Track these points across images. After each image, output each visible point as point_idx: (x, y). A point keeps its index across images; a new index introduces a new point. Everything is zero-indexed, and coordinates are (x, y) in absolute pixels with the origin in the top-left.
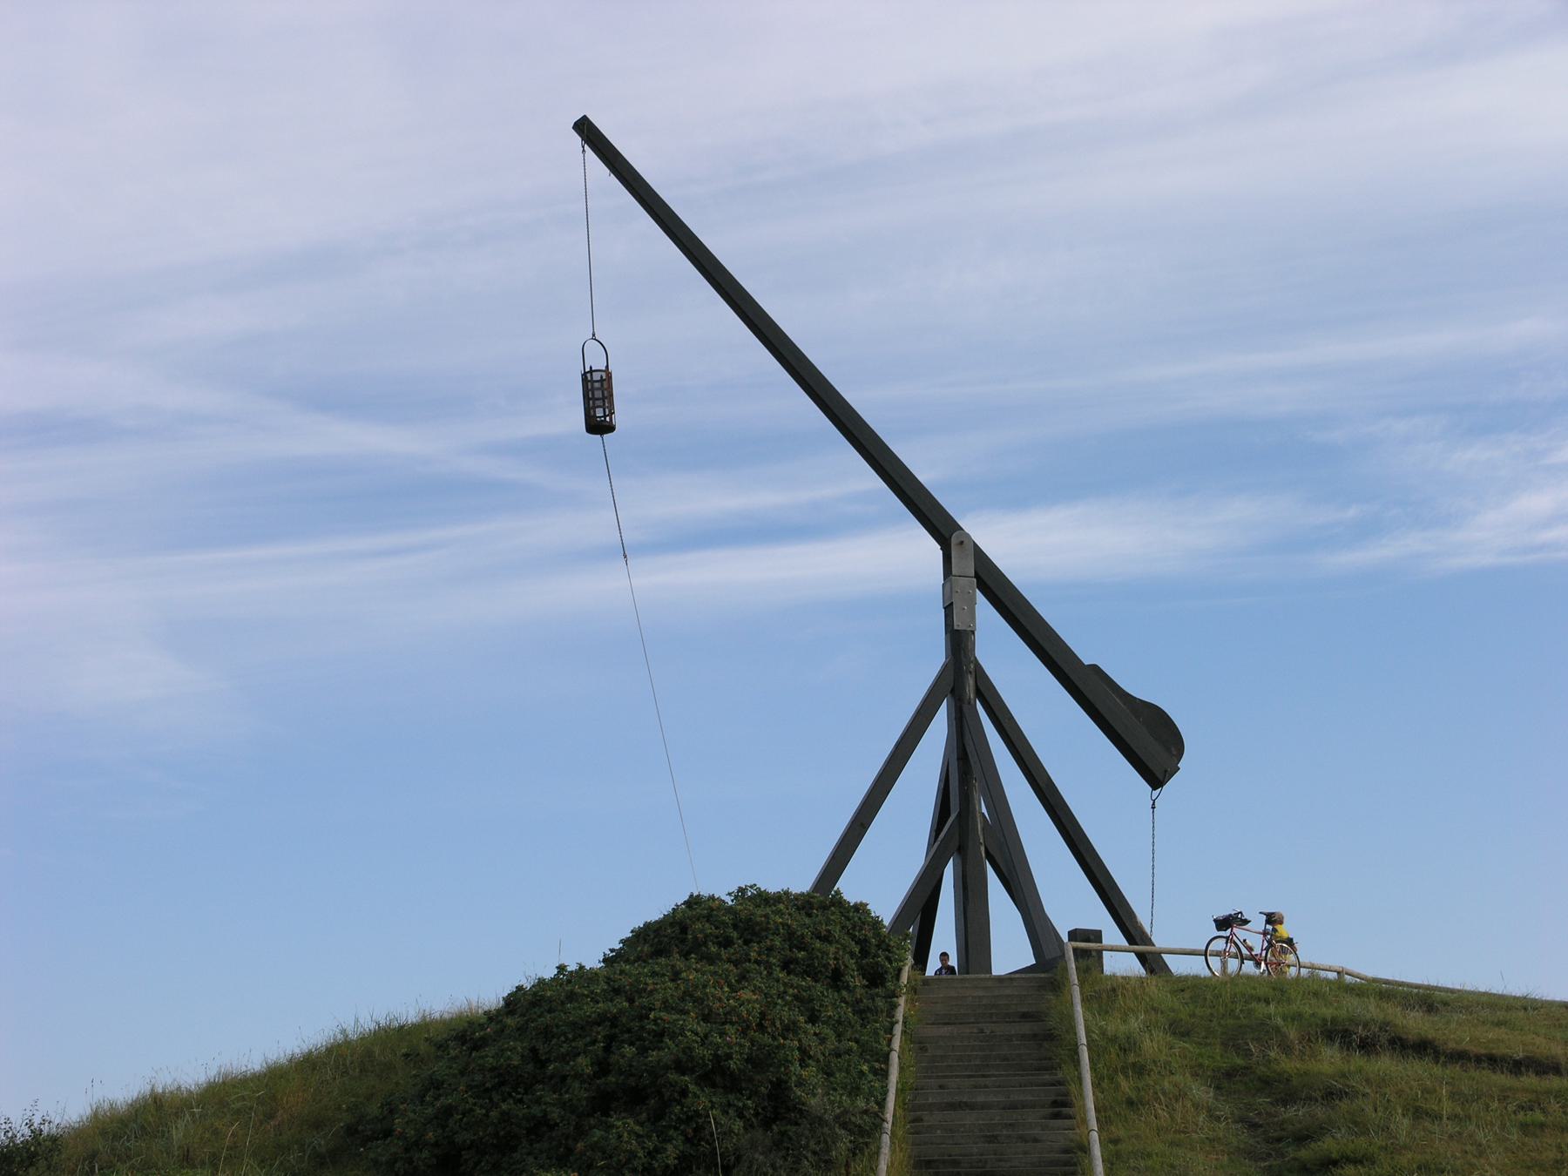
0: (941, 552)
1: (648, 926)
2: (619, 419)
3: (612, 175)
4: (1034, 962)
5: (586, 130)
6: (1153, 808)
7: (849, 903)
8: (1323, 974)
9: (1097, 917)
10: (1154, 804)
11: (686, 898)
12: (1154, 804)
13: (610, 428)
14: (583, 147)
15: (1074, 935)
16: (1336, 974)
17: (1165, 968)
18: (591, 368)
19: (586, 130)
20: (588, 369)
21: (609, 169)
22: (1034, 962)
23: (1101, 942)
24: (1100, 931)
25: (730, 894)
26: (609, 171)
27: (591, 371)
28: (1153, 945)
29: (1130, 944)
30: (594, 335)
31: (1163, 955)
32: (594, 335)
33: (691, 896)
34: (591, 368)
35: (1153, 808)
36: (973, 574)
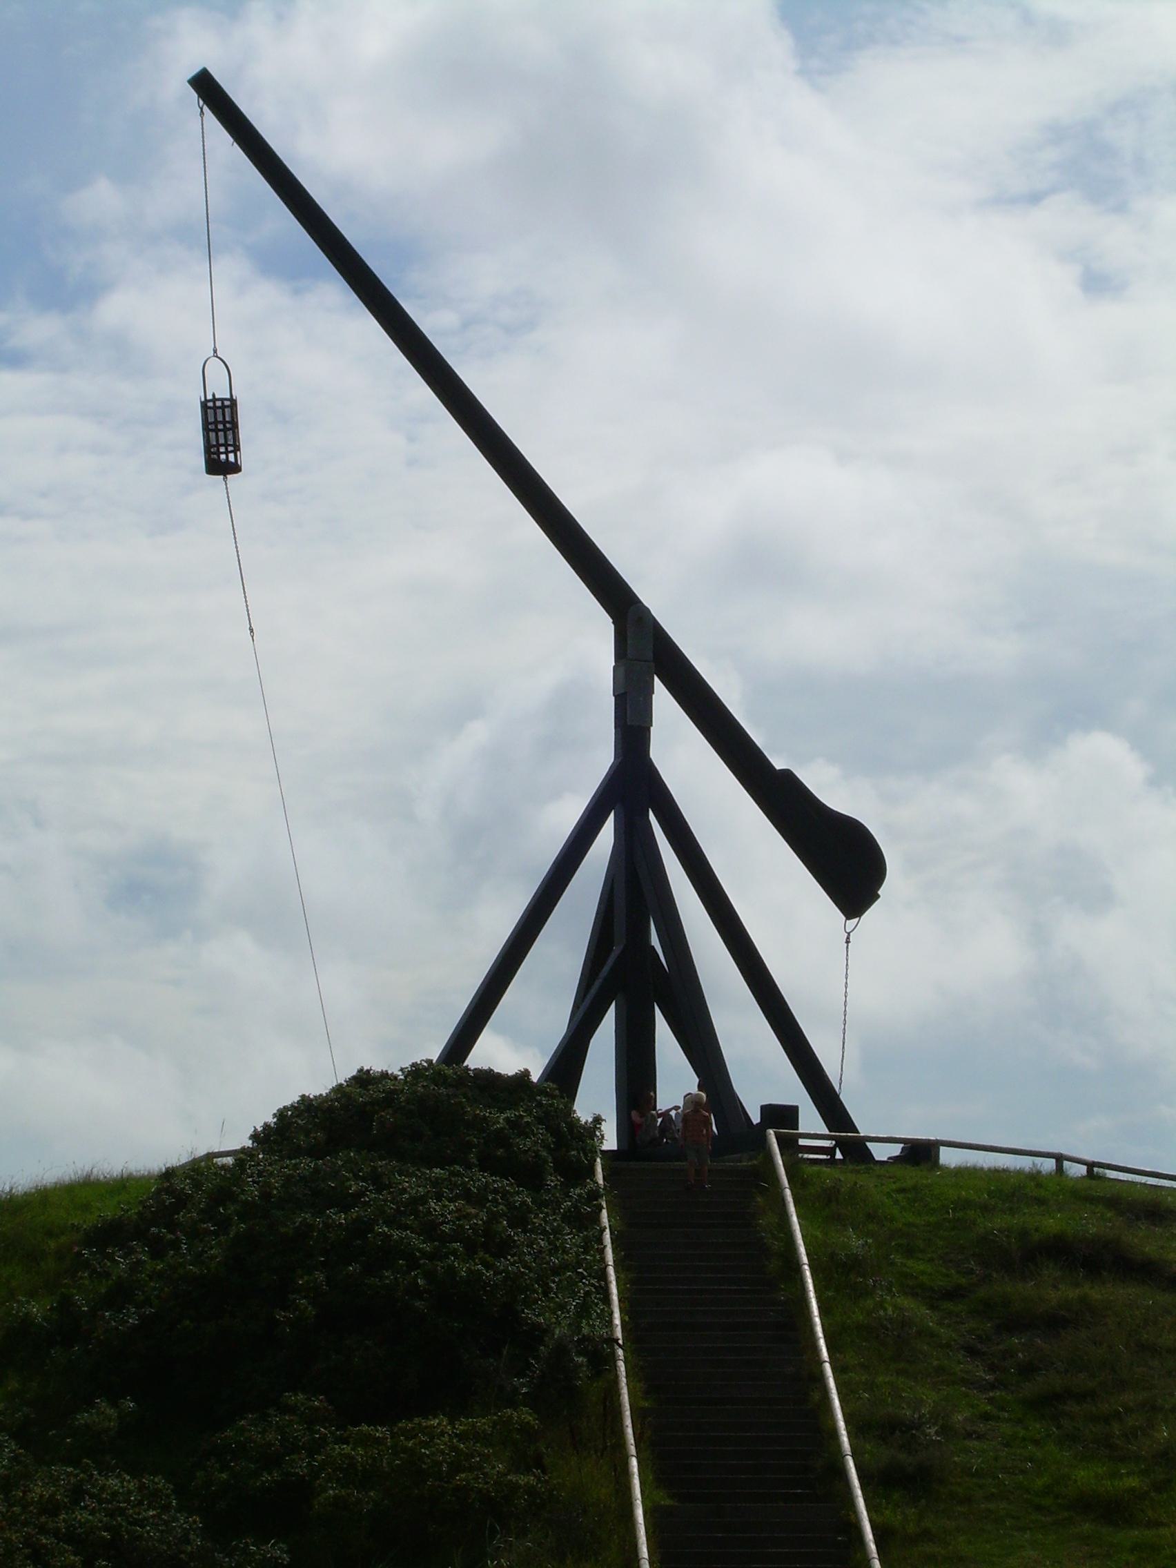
1: (306, 1106)
2: (246, 456)
3: (235, 144)
4: (615, 1148)
5: (206, 86)
6: (848, 942)
9: (791, 1090)
10: (848, 938)
11: (354, 1073)
12: (848, 938)
13: (235, 468)
14: (202, 109)
15: (768, 1111)
16: (1053, 1161)
17: (868, 1155)
18: (214, 395)
19: (206, 86)
20: (209, 397)
21: (233, 137)
22: (615, 1148)
23: (797, 1129)
24: (797, 1108)
25: (402, 1070)
28: (858, 1132)
30: (215, 351)
31: (868, 1144)
32: (215, 351)
34: (214, 395)
35: (848, 942)
36: (650, 655)
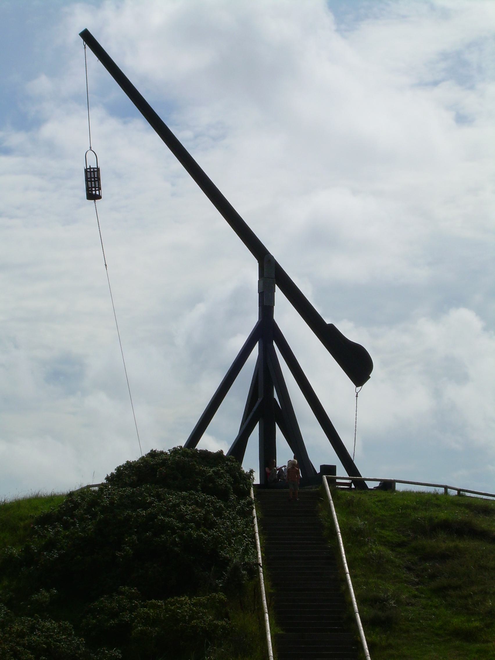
0: (258, 263)
1: (129, 465)
2: (104, 192)
3: (99, 60)
4: (259, 483)
5: (87, 36)
6: (357, 396)
7: (181, 447)
8: (93, 489)
9: (333, 459)
10: (357, 395)
11: (149, 452)
12: (357, 395)
13: (99, 197)
14: (85, 46)
15: (323, 468)
17: (365, 486)
18: (90, 166)
19: (87, 36)
20: (88, 167)
21: (98, 58)
22: (259, 483)
23: (336, 475)
24: (335, 466)
26: (98, 59)
27: (90, 168)
28: (361, 477)
29: (350, 476)
30: (91, 148)
31: (365, 482)
32: (91, 148)
33: (152, 451)
34: (90, 166)
35: (357, 396)
